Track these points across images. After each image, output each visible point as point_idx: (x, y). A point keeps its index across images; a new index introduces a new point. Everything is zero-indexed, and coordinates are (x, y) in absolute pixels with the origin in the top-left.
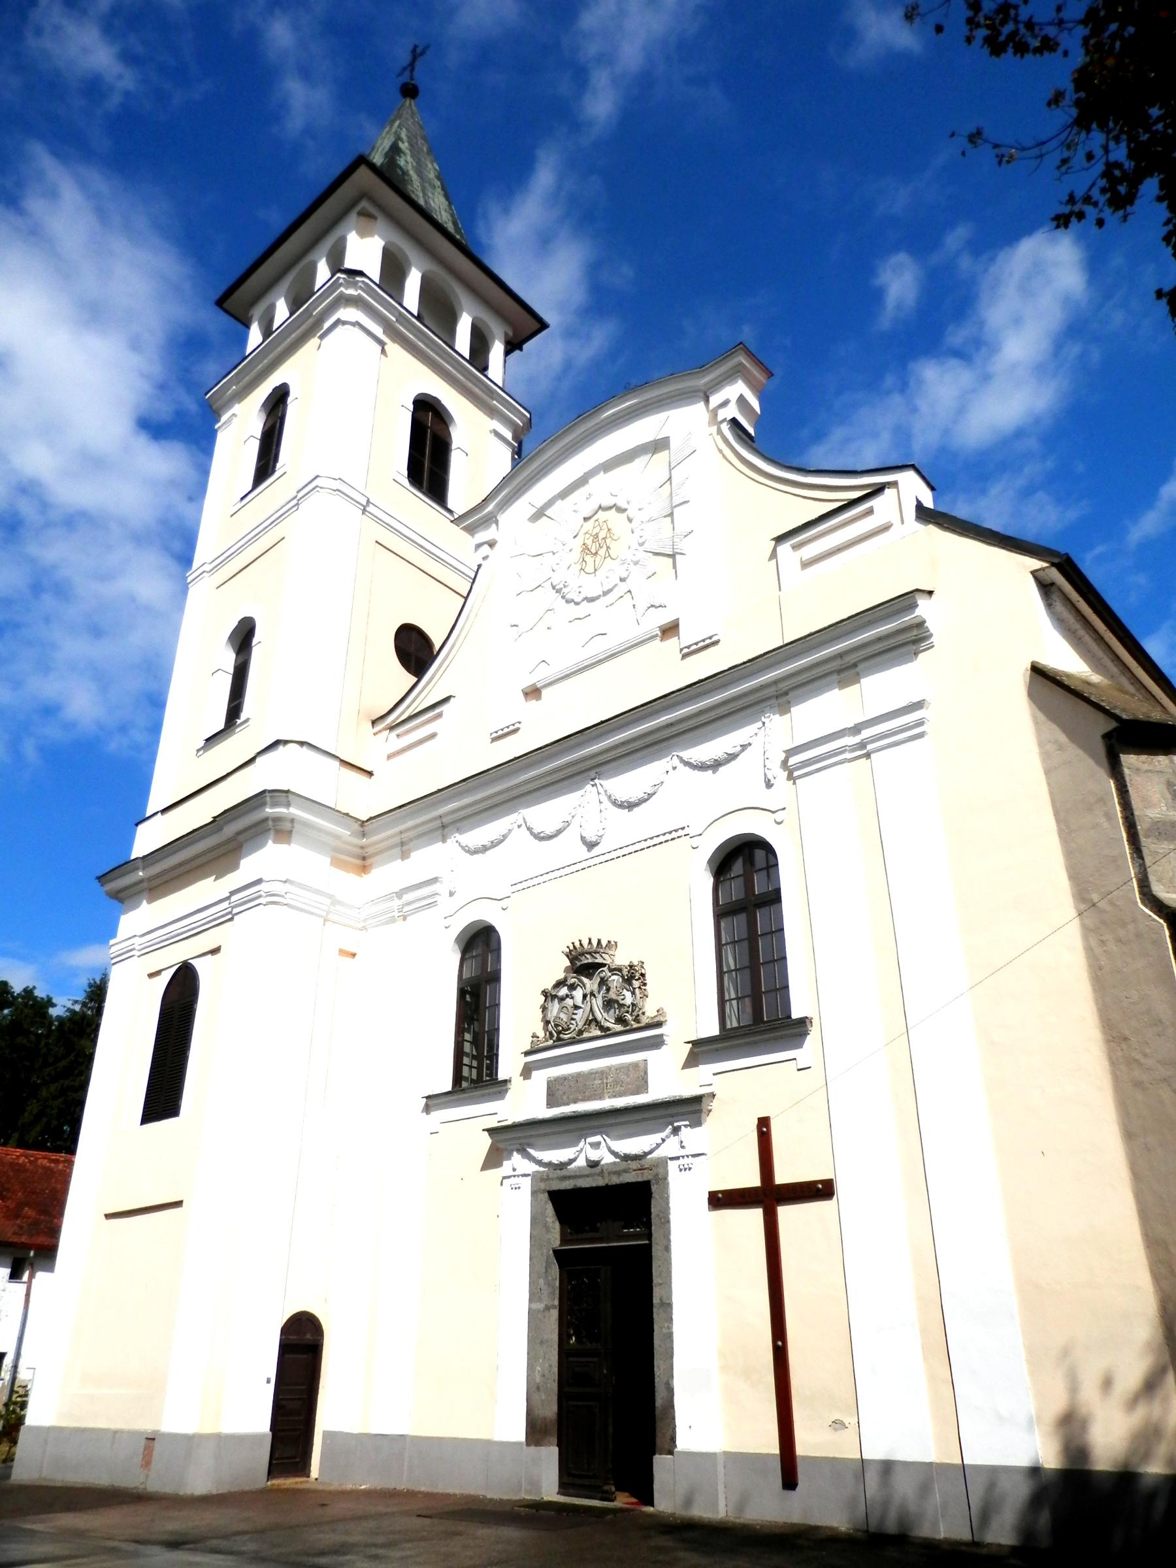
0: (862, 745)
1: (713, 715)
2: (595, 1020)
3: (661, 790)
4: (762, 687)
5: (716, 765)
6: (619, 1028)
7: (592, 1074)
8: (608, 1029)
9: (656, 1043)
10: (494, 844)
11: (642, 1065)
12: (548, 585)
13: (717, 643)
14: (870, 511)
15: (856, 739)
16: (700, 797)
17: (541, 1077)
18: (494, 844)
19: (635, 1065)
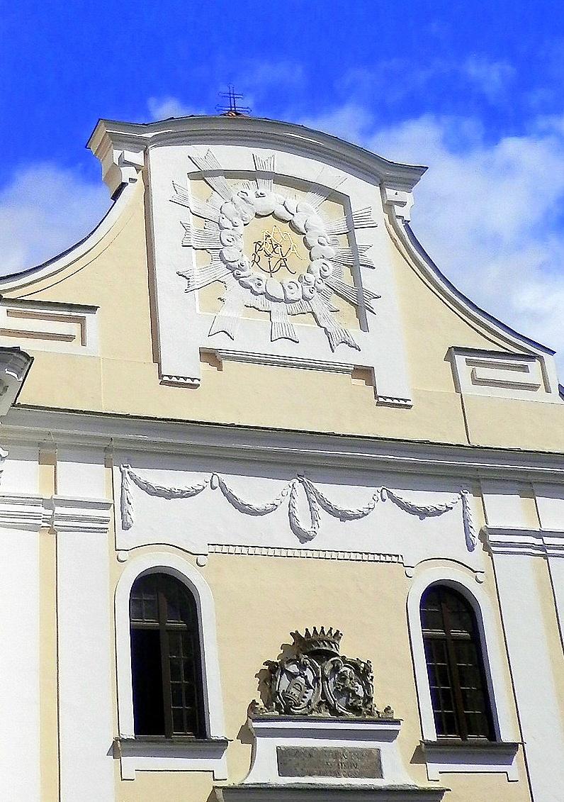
0: (543, 547)
1: (432, 471)
2: (327, 703)
3: (372, 512)
4: (467, 468)
5: (423, 513)
6: (351, 715)
7: (325, 752)
8: (342, 714)
9: (390, 736)
10: (183, 495)
11: (375, 753)
12: (219, 251)
13: (409, 407)
14: (524, 369)
15: (539, 542)
16: (426, 538)
17: (267, 747)
18: (183, 495)
19: (369, 752)
